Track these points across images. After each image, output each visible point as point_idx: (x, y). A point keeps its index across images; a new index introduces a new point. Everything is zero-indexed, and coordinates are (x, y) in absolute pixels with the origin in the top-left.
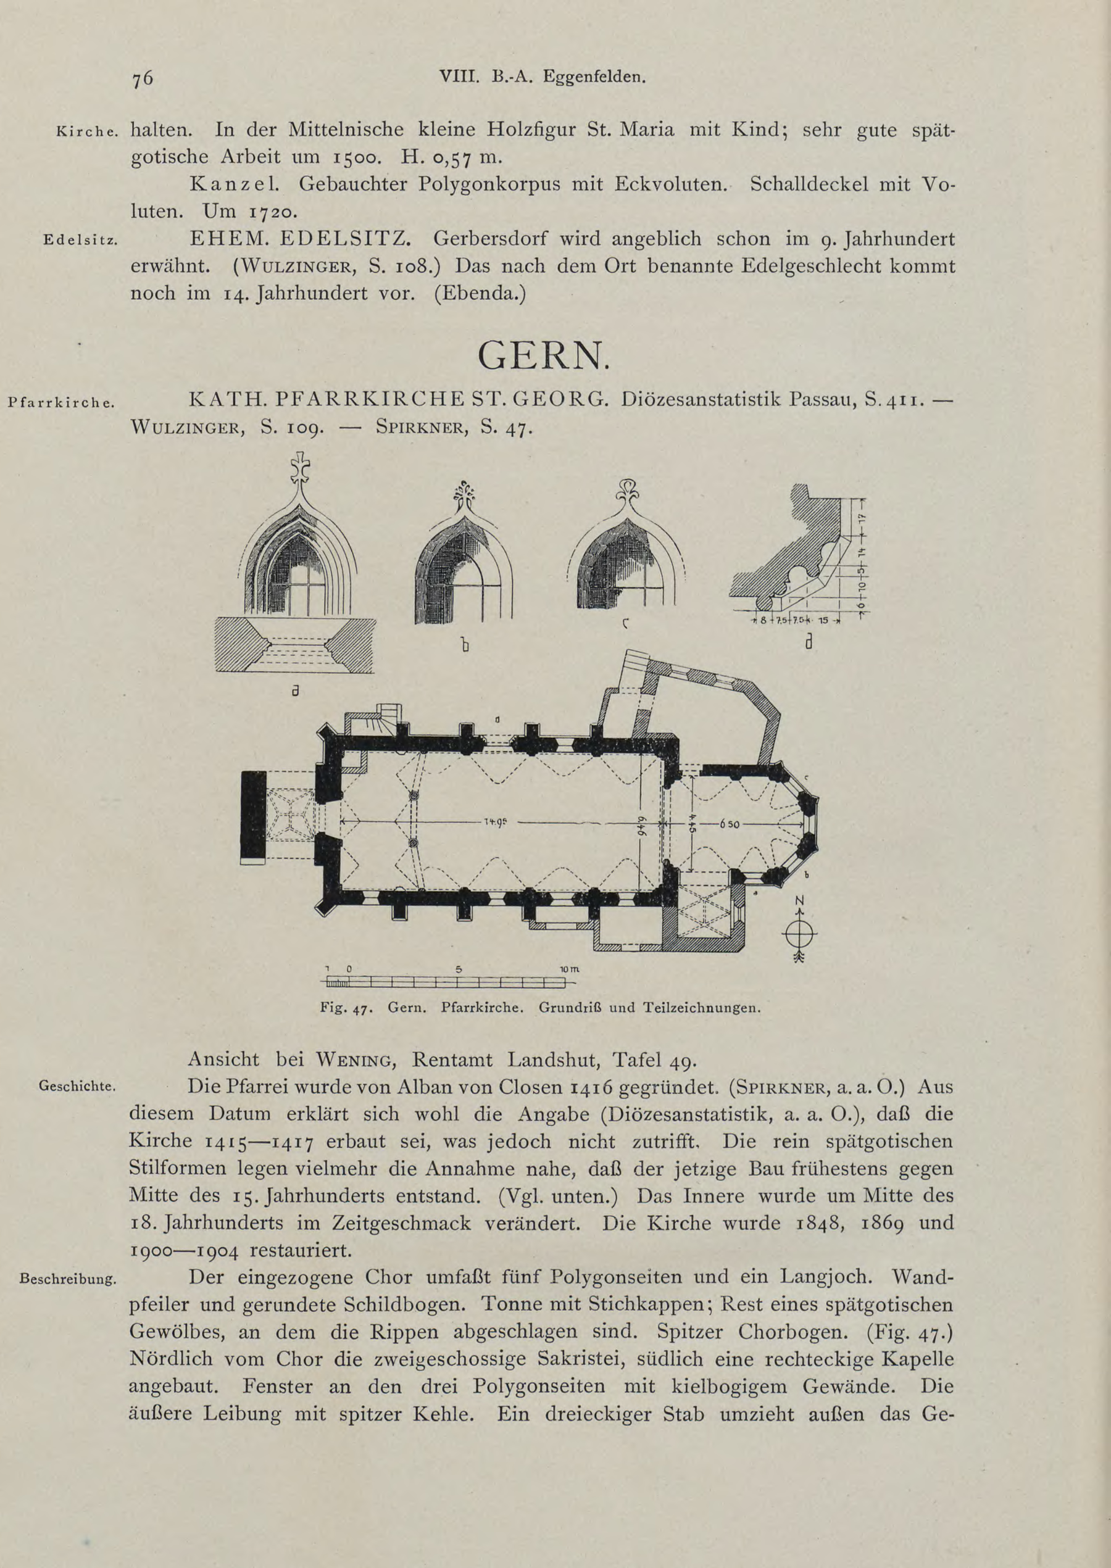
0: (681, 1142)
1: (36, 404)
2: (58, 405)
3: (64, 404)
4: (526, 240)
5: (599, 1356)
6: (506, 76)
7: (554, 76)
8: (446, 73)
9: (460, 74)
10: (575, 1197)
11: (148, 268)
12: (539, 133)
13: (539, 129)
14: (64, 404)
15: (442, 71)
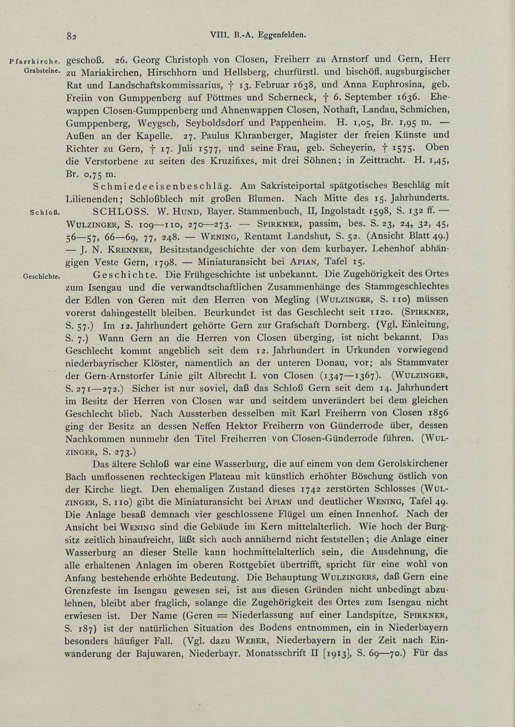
0: (312, 565)
1: (23, 62)
2: (33, 63)
3: (36, 62)
4: (234, 124)
5: (327, 134)
6: (240, 35)
7: (263, 35)
8: (213, 33)
9: (220, 34)
10: (288, 363)
11: (184, 288)
12: (132, 642)
13: (132, 641)
14: (36, 62)
15: (212, 32)
